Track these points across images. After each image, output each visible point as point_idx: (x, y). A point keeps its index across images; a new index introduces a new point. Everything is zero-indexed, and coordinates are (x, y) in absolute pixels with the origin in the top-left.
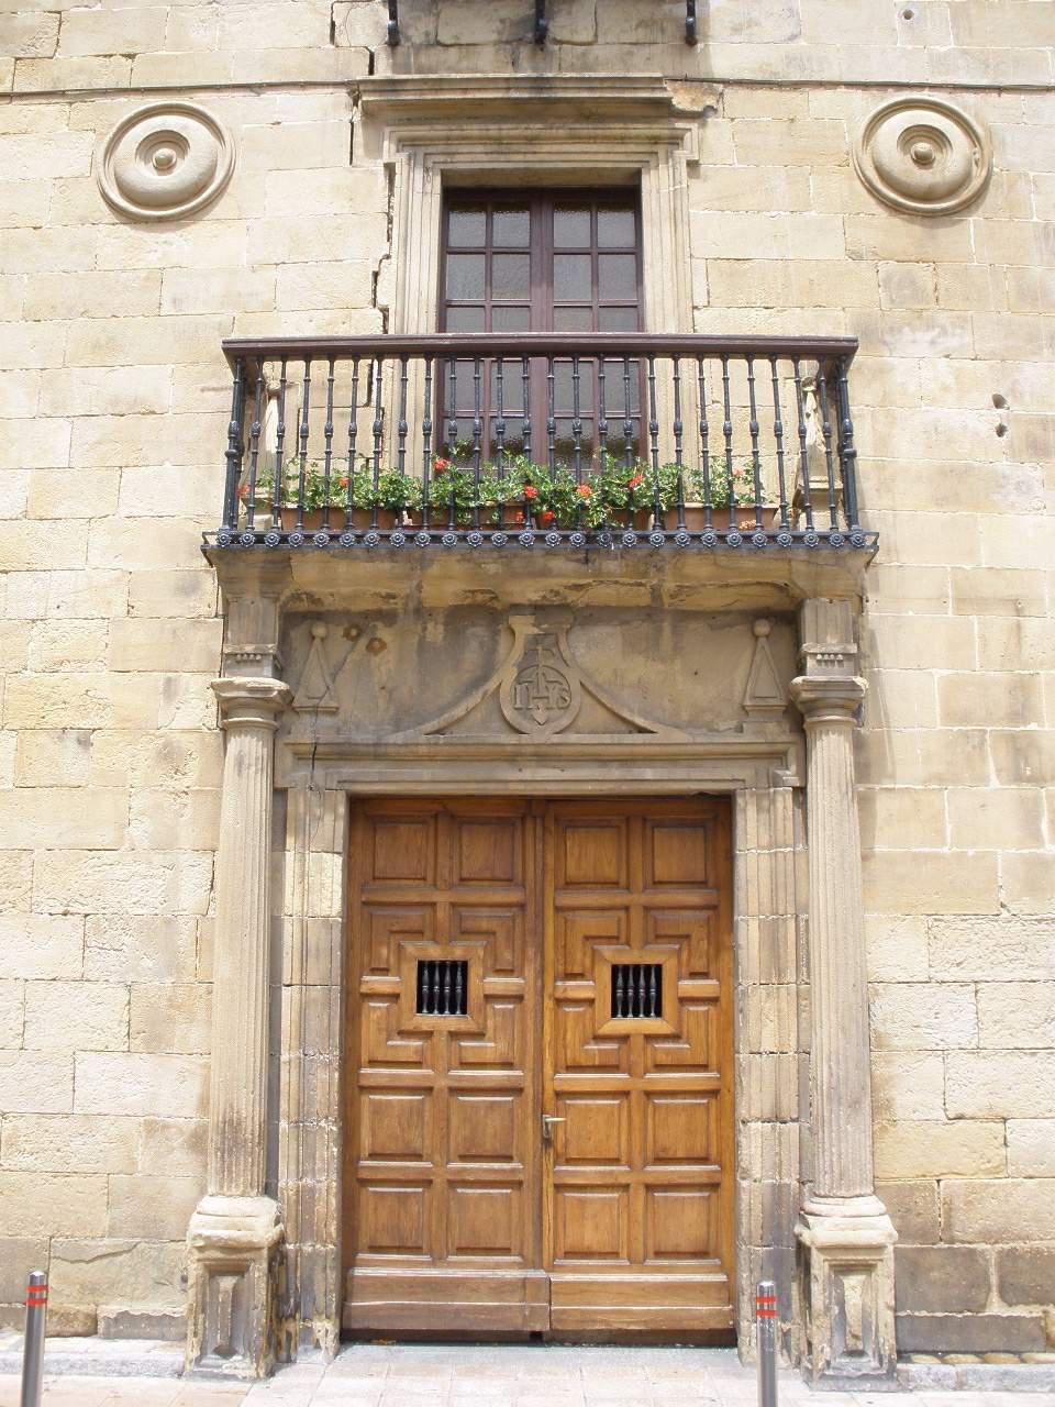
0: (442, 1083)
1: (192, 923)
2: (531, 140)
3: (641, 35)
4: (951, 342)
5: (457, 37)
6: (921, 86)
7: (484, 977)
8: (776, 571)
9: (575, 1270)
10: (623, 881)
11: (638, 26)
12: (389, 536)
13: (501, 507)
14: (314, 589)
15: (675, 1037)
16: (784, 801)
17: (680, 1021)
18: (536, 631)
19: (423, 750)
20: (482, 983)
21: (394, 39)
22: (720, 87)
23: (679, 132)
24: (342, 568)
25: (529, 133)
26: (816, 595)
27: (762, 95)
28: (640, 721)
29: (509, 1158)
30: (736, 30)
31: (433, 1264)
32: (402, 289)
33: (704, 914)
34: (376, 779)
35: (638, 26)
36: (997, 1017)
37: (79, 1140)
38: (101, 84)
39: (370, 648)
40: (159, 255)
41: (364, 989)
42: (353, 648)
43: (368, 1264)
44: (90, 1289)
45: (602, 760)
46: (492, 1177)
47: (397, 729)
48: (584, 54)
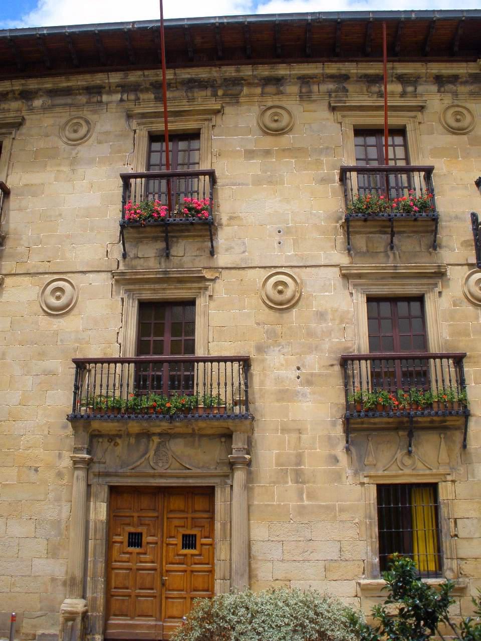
0: (135, 567)
1: (65, 522)
2: (164, 289)
3: (198, 253)
4: (285, 350)
5: (143, 255)
6: (282, 267)
7: (147, 537)
8: (224, 424)
9: (170, 622)
10: (186, 510)
11: (197, 250)
13: (147, 408)
14: (98, 429)
15: (200, 555)
16: (228, 489)
17: (201, 550)
18: (160, 440)
19: (128, 474)
20: (146, 539)
21: (124, 256)
22: (221, 270)
23: (207, 286)
24: (105, 424)
25: (163, 287)
26: (236, 431)
27: (233, 271)
28: (187, 466)
29: (152, 589)
30: (227, 250)
31: (130, 620)
32: (125, 338)
33: (209, 520)
34: (116, 481)
35: (197, 250)
36: (289, 551)
37: (32, 584)
38: (41, 271)
39: (114, 445)
40: (57, 326)
41: (114, 540)
42: (110, 445)
43: (113, 620)
44: (34, 626)
45: (178, 477)
46: (147, 594)
47: (122, 467)
48: (181, 260)
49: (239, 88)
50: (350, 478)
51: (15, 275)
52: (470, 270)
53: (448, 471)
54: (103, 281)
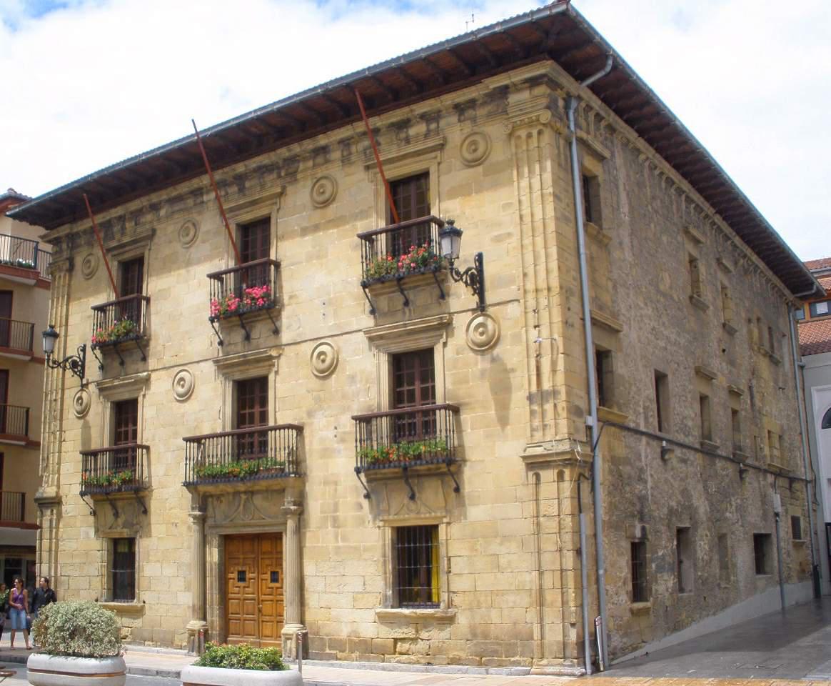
4: (327, 413)
12: (590, 414)
20: (249, 575)
29: (253, 615)
41: (229, 577)
45: (259, 526)
49: (296, 165)
50: (371, 522)
51: (157, 370)
52: (473, 314)
53: (444, 514)
54: (209, 368)
